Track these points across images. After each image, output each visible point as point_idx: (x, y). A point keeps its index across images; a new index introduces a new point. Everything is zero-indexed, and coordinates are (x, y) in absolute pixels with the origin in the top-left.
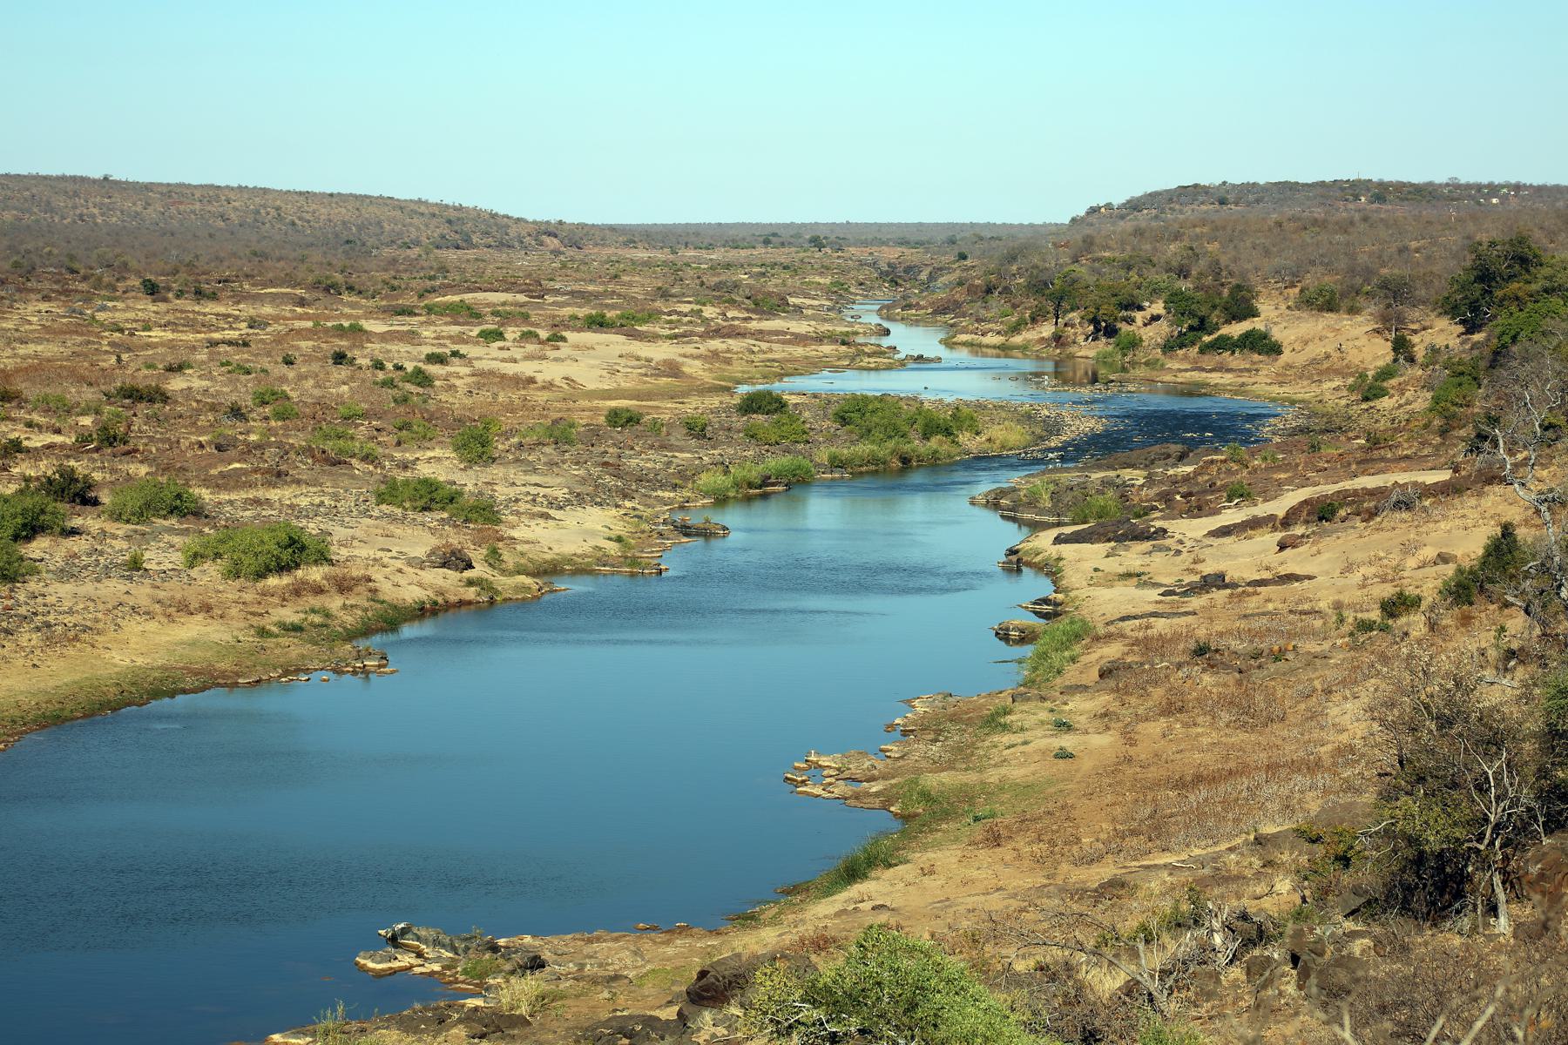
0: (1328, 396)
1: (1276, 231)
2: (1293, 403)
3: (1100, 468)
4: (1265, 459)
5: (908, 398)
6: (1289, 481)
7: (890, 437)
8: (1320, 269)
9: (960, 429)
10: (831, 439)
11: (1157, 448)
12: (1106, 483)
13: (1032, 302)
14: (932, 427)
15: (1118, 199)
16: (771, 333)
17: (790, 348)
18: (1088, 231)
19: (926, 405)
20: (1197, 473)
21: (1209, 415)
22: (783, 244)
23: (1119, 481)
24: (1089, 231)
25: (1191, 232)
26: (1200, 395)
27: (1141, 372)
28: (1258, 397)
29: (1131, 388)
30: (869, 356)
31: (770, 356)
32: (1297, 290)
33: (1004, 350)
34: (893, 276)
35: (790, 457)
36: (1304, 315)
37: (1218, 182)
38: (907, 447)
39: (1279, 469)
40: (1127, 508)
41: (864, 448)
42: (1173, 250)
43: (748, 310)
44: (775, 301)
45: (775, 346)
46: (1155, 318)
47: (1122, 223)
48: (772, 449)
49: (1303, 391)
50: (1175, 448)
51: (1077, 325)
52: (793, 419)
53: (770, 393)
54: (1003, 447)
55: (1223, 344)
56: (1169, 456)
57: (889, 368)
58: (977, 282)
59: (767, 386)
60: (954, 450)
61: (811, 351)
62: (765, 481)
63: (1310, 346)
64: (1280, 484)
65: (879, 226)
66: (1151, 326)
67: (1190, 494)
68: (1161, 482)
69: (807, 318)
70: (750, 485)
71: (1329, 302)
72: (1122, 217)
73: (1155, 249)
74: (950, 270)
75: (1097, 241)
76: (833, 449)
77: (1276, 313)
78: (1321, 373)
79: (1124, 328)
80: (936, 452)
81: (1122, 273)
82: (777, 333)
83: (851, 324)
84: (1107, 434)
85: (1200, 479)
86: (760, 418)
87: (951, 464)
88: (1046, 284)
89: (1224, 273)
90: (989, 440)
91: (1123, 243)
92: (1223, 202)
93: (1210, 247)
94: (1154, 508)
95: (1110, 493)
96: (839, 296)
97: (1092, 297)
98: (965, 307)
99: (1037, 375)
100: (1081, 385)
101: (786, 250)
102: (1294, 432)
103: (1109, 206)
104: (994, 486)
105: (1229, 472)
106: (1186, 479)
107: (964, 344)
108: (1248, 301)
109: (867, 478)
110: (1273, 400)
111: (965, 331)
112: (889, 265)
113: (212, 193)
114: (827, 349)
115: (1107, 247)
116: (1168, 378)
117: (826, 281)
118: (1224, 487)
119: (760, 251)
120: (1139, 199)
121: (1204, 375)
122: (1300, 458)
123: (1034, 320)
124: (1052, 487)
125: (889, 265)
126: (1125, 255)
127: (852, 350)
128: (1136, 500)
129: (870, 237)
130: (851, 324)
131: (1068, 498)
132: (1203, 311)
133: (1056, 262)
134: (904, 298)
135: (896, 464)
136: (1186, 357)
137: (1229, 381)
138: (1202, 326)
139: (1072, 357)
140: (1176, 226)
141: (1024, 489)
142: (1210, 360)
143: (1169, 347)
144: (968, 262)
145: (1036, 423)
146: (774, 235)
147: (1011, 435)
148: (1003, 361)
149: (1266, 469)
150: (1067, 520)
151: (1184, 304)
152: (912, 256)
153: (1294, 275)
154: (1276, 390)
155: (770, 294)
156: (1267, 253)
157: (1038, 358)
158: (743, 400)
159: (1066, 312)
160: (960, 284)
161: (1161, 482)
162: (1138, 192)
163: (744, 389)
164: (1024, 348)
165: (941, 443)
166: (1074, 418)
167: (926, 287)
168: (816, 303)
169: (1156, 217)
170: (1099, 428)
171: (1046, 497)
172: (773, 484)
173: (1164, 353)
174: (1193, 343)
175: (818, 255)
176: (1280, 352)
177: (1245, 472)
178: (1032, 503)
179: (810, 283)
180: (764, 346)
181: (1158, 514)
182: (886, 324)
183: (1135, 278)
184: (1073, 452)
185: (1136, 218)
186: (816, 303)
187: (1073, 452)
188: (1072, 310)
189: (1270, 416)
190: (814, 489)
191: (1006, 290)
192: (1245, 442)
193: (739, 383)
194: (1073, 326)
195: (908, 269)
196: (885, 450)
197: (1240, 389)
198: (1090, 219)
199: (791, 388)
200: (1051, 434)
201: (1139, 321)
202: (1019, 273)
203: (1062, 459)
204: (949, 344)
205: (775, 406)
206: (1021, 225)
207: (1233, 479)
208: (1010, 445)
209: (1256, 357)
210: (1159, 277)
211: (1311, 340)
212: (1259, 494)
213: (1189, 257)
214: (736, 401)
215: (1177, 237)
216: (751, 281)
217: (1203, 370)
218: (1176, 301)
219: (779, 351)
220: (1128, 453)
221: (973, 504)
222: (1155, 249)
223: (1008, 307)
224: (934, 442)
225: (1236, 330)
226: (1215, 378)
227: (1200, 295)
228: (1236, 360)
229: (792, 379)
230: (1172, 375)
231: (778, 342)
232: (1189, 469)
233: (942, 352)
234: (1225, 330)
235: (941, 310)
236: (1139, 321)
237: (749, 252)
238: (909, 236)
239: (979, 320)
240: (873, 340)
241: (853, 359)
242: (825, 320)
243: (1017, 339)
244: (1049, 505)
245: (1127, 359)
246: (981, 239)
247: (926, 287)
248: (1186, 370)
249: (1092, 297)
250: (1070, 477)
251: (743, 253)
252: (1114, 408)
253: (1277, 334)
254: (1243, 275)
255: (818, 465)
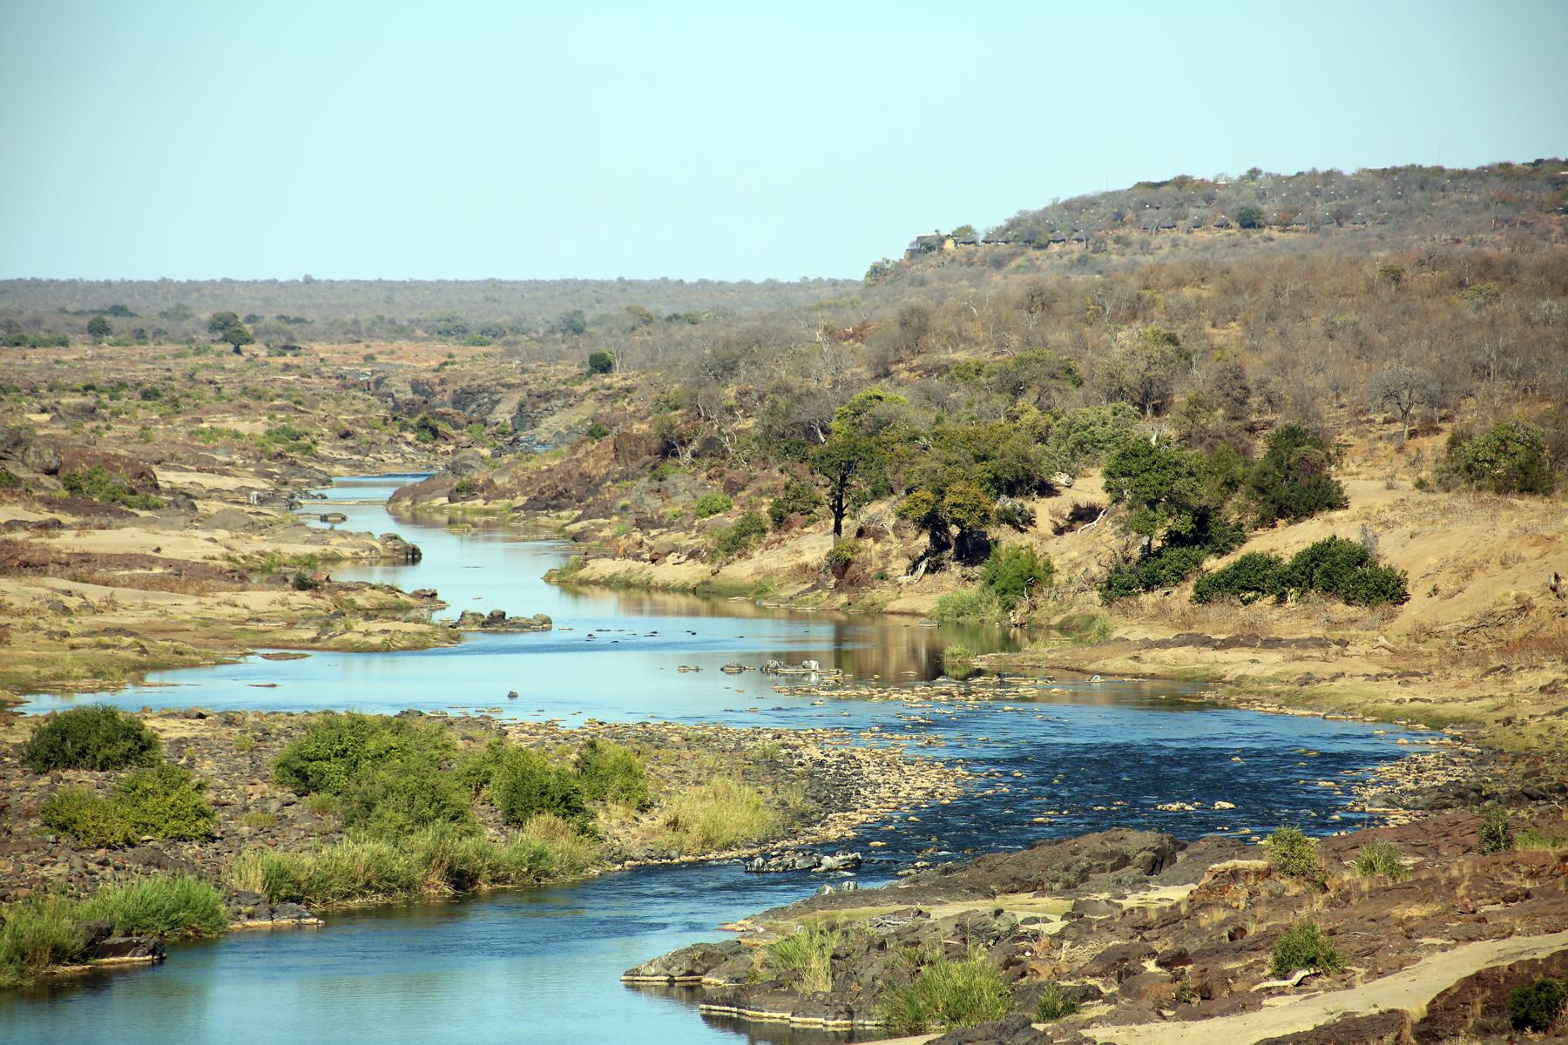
0: (1525, 708)
1: (1387, 291)
2: (1437, 724)
3: (951, 891)
4: (1370, 867)
5: (468, 722)
6: (1434, 925)
7: (423, 821)
8: (1501, 387)
9: (599, 796)
10: (271, 829)
11: (1093, 841)
12: (966, 930)
13: (775, 477)
14: (528, 795)
15: (987, 219)
16: (110, 560)
17: (163, 600)
18: (914, 298)
19: (514, 739)
20: (1198, 904)
21: (1222, 756)
22: (140, 335)
23: (1001, 925)
24: (910, 304)
25: (1171, 298)
26: (1201, 707)
27: (1049, 649)
28: (1348, 709)
29: (1026, 688)
30: (368, 615)
31: (111, 619)
32: (1441, 441)
33: (708, 596)
34: (424, 414)
35: (161, 877)
36: (1462, 502)
37: (1236, 171)
38: (466, 847)
39: (1408, 892)
40: (1023, 993)
41: (358, 851)
42: (1125, 344)
43: (50, 504)
44: (123, 479)
45: (122, 594)
46: (1084, 514)
47: (997, 277)
48: (116, 858)
49: (1464, 694)
50: (1139, 841)
51: (888, 531)
52: (171, 780)
53: (110, 714)
54: (708, 841)
55: (1255, 579)
56: (1124, 861)
57: (418, 647)
58: (639, 428)
59: (103, 699)
60: (585, 850)
61: (222, 604)
62: (97, 943)
63: (1479, 582)
64: (1410, 933)
65: (389, 290)
66: (1073, 537)
67: (1181, 958)
68: (1107, 927)
69: (206, 521)
70: (60, 954)
71: (1524, 470)
72: (998, 263)
73: (1081, 342)
74: (571, 400)
75: (937, 323)
76: (277, 856)
77: (1390, 498)
78: (1506, 649)
79: (1006, 538)
80: (539, 856)
81: (1000, 401)
82: (128, 560)
83: (319, 537)
84: (969, 806)
85: (1205, 919)
86: (83, 780)
87: (572, 889)
88: (809, 432)
89: (1255, 401)
90: (674, 824)
91: (1001, 326)
92: (1250, 221)
93: (1219, 336)
94: (1091, 994)
95: (980, 956)
96: (289, 462)
97: (925, 462)
98: (609, 491)
99: (792, 659)
100: (901, 682)
101: (150, 349)
102: (1442, 799)
103: (964, 236)
104: (689, 940)
105: (1278, 900)
106: (1171, 918)
107: (608, 583)
108: (1315, 468)
109: (361, 928)
110: (1388, 718)
111: (609, 550)
112: (416, 386)
113: (415, 286)
114: (259, 599)
115: (959, 339)
116: (1119, 663)
117: (254, 427)
118: (1268, 938)
119: (81, 349)
120: (1039, 217)
121: (1209, 655)
122: (1462, 867)
123: (780, 521)
124: (834, 942)
125: (416, 386)
126: (1007, 358)
127: (325, 602)
128: (1045, 972)
129: (366, 316)
130: (319, 537)
131: (873, 968)
132: (1205, 494)
133: (832, 378)
134: (454, 469)
135: (438, 888)
136: (1162, 612)
137: (1280, 673)
138: (1202, 532)
139: (876, 612)
140: (1134, 282)
141: (763, 946)
142: (1224, 618)
143: (1120, 586)
144: (615, 379)
145: (791, 779)
146: (118, 311)
147: (729, 811)
148: (708, 627)
149: (1374, 894)
150: (870, 1024)
151: (1153, 478)
152: (473, 364)
153: (1432, 402)
154: (1392, 693)
155: (108, 462)
156: (1363, 348)
157: (793, 616)
158: (40, 734)
159: (861, 501)
160: (596, 433)
161: (1107, 927)
162: (1036, 200)
163: (41, 706)
164: (757, 592)
165: (551, 833)
166: (885, 765)
167: (510, 439)
168: (229, 483)
169: (1083, 261)
170: (949, 792)
171: (818, 965)
172: (118, 950)
173: (1108, 601)
174: (1180, 576)
175: (232, 362)
176: (1400, 598)
177: (1320, 900)
178: (784, 983)
179: (214, 433)
180: (95, 594)
181: (1099, 1009)
182: (409, 536)
183: (1032, 415)
184: (884, 852)
185: (1031, 266)
186: (229, 483)
187: (884, 852)
188: (876, 495)
189: (1378, 758)
190: (226, 960)
191: (712, 447)
192: (1322, 824)
193: (28, 689)
194: (878, 535)
195: (464, 398)
196: (414, 852)
197: (1302, 692)
198: (917, 269)
199: (162, 701)
200: (827, 805)
201: (1044, 522)
202: (744, 403)
203: (856, 866)
204: (569, 583)
205: (124, 746)
206: (746, 286)
207: (1288, 918)
208: (727, 836)
209: (1339, 609)
210: (1089, 411)
211: (1483, 566)
212: (1357, 957)
213: (1166, 362)
214: (22, 735)
215: (1135, 310)
216: (59, 430)
217: (1207, 642)
218: (1137, 472)
219: (135, 608)
220: (1022, 853)
221: (633, 986)
222: (1081, 342)
223: (715, 490)
224: (537, 832)
225: (1287, 542)
226: (1236, 663)
227: (1195, 455)
228: (1288, 618)
229: (168, 677)
230: (1137, 666)
231: (132, 583)
232: (1177, 894)
233: (552, 603)
234: (1260, 543)
235: (548, 498)
236: (1044, 522)
237: (52, 353)
238: (458, 315)
239: (643, 523)
240: (377, 576)
241: (326, 625)
242: (253, 527)
243: (741, 571)
244: (825, 986)
245: (1015, 618)
246: (648, 320)
247: (510, 439)
248: (1164, 644)
249: (925, 462)
250: (877, 912)
251: (36, 357)
252: (987, 740)
253: (1392, 552)
254: (1303, 406)
255: (233, 896)
